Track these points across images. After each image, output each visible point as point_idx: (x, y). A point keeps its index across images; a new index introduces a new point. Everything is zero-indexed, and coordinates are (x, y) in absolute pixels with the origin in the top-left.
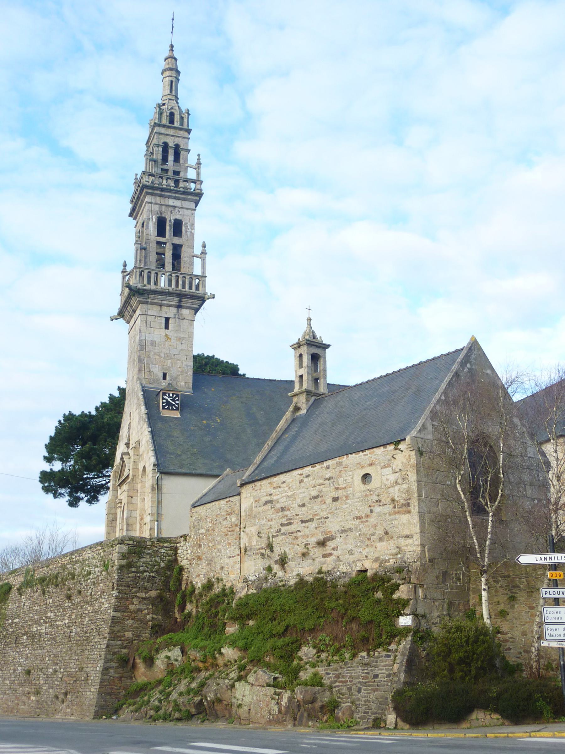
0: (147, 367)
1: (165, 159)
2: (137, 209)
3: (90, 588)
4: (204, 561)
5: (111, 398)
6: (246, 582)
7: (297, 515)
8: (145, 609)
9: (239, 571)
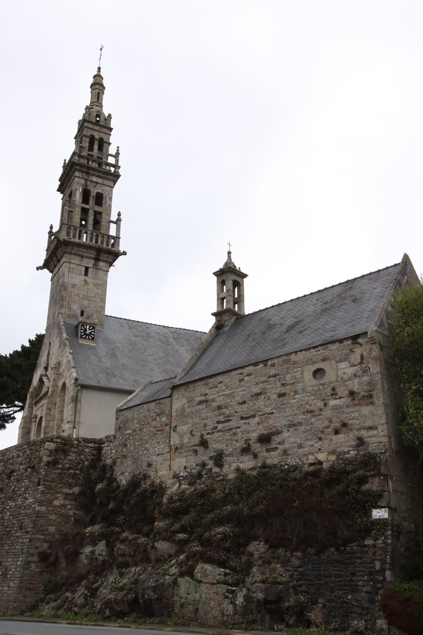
0: (68, 304)
1: (91, 148)
2: (65, 184)
3: (13, 484)
4: (129, 459)
5: (23, 347)
6: (177, 478)
7: (236, 412)
8: (68, 505)
9: (168, 467)
